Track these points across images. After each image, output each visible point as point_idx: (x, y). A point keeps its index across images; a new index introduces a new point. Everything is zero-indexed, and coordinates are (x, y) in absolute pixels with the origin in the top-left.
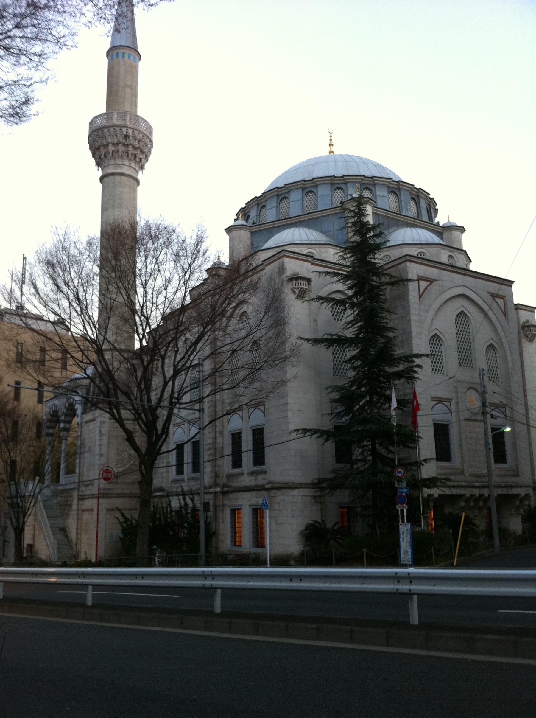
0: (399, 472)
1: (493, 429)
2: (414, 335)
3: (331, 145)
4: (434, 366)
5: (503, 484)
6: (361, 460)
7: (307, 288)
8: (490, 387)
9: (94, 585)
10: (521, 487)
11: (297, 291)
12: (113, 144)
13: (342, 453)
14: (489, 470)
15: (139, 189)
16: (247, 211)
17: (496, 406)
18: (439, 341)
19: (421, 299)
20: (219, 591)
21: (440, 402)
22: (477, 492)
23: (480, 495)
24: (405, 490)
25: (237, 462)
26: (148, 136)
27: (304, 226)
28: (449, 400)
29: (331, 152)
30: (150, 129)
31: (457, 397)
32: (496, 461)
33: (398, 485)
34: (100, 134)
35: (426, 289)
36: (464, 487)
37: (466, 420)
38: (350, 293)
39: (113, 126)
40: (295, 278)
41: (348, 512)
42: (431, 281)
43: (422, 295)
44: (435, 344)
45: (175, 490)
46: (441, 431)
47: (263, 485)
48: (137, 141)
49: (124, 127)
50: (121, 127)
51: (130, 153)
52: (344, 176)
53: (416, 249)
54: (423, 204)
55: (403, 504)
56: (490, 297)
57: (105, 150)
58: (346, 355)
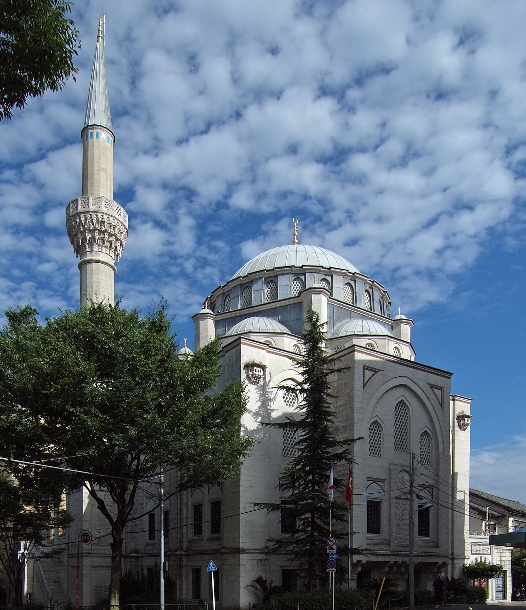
1: (419, 507)
2: (356, 420)
4: (372, 450)
5: (424, 554)
6: (301, 531)
8: (420, 469)
10: (439, 556)
13: (287, 524)
14: (411, 540)
16: (214, 300)
17: (425, 487)
18: (379, 428)
21: (375, 482)
22: (400, 560)
23: (403, 562)
24: (335, 557)
25: (198, 530)
26: (123, 223)
27: (266, 316)
28: (383, 481)
31: (390, 478)
32: (420, 534)
33: (330, 552)
35: (371, 377)
36: (389, 555)
37: (396, 498)
38: (301, 379)
39: (89, 212)
40: (251, 366)
41: (287, 575)
43: (366, 384)
44: (375, 430)
45: (148, 552)
46: (374, 508)
47: (218, 550)
48: (112, 227)
49: (99, 212)
51: (106, 240)
52: (303, 266)
55: (333, 568)
56: (428, 387)
58: (295, 438)
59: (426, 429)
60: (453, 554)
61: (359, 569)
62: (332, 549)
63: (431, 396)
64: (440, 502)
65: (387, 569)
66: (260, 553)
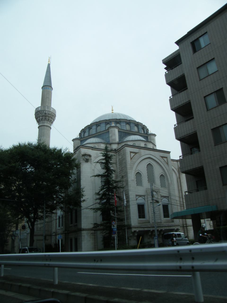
0: (113, 223)
3: (112, 110)
5: (167, 225)
7: (89, 158)
9: (59, 267)
11: (85, 160)
12: (42, 116)
15: (51, 130)
19: (132, 160)
20: (56, 269)
29: (112, 112)
30: (55, 110)
34: (37, 113)
35: (134, 156)
40: (84, 155)
42: (136, 153)
43: (132, 158)
46: (141, 208)
48: (49, 115)
50: (44, 111)
53: (132, 142)
54: (140, 127)
57: (39, 119)
59: (162, 174)
60: (186, 224)
61: (136, 234)
62: (114, 226)
63: (162, 161)
64: (172, 203)
65: (150, 234)
66: (91, 230)
